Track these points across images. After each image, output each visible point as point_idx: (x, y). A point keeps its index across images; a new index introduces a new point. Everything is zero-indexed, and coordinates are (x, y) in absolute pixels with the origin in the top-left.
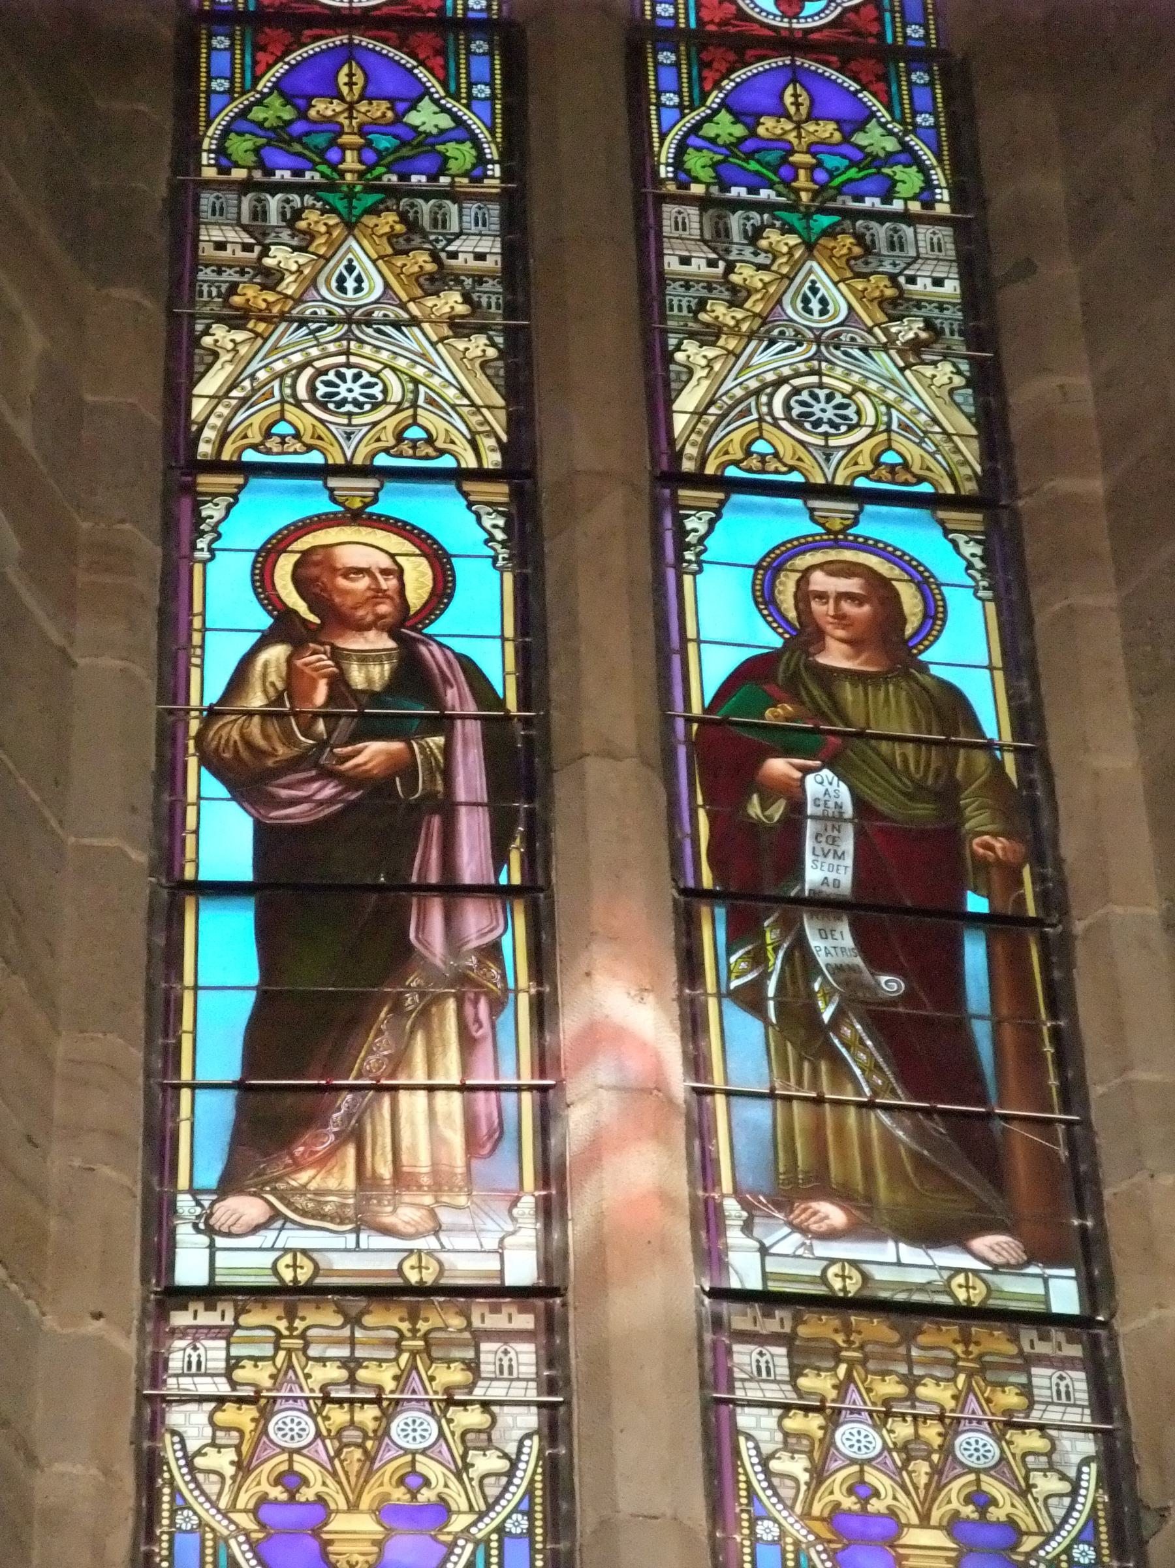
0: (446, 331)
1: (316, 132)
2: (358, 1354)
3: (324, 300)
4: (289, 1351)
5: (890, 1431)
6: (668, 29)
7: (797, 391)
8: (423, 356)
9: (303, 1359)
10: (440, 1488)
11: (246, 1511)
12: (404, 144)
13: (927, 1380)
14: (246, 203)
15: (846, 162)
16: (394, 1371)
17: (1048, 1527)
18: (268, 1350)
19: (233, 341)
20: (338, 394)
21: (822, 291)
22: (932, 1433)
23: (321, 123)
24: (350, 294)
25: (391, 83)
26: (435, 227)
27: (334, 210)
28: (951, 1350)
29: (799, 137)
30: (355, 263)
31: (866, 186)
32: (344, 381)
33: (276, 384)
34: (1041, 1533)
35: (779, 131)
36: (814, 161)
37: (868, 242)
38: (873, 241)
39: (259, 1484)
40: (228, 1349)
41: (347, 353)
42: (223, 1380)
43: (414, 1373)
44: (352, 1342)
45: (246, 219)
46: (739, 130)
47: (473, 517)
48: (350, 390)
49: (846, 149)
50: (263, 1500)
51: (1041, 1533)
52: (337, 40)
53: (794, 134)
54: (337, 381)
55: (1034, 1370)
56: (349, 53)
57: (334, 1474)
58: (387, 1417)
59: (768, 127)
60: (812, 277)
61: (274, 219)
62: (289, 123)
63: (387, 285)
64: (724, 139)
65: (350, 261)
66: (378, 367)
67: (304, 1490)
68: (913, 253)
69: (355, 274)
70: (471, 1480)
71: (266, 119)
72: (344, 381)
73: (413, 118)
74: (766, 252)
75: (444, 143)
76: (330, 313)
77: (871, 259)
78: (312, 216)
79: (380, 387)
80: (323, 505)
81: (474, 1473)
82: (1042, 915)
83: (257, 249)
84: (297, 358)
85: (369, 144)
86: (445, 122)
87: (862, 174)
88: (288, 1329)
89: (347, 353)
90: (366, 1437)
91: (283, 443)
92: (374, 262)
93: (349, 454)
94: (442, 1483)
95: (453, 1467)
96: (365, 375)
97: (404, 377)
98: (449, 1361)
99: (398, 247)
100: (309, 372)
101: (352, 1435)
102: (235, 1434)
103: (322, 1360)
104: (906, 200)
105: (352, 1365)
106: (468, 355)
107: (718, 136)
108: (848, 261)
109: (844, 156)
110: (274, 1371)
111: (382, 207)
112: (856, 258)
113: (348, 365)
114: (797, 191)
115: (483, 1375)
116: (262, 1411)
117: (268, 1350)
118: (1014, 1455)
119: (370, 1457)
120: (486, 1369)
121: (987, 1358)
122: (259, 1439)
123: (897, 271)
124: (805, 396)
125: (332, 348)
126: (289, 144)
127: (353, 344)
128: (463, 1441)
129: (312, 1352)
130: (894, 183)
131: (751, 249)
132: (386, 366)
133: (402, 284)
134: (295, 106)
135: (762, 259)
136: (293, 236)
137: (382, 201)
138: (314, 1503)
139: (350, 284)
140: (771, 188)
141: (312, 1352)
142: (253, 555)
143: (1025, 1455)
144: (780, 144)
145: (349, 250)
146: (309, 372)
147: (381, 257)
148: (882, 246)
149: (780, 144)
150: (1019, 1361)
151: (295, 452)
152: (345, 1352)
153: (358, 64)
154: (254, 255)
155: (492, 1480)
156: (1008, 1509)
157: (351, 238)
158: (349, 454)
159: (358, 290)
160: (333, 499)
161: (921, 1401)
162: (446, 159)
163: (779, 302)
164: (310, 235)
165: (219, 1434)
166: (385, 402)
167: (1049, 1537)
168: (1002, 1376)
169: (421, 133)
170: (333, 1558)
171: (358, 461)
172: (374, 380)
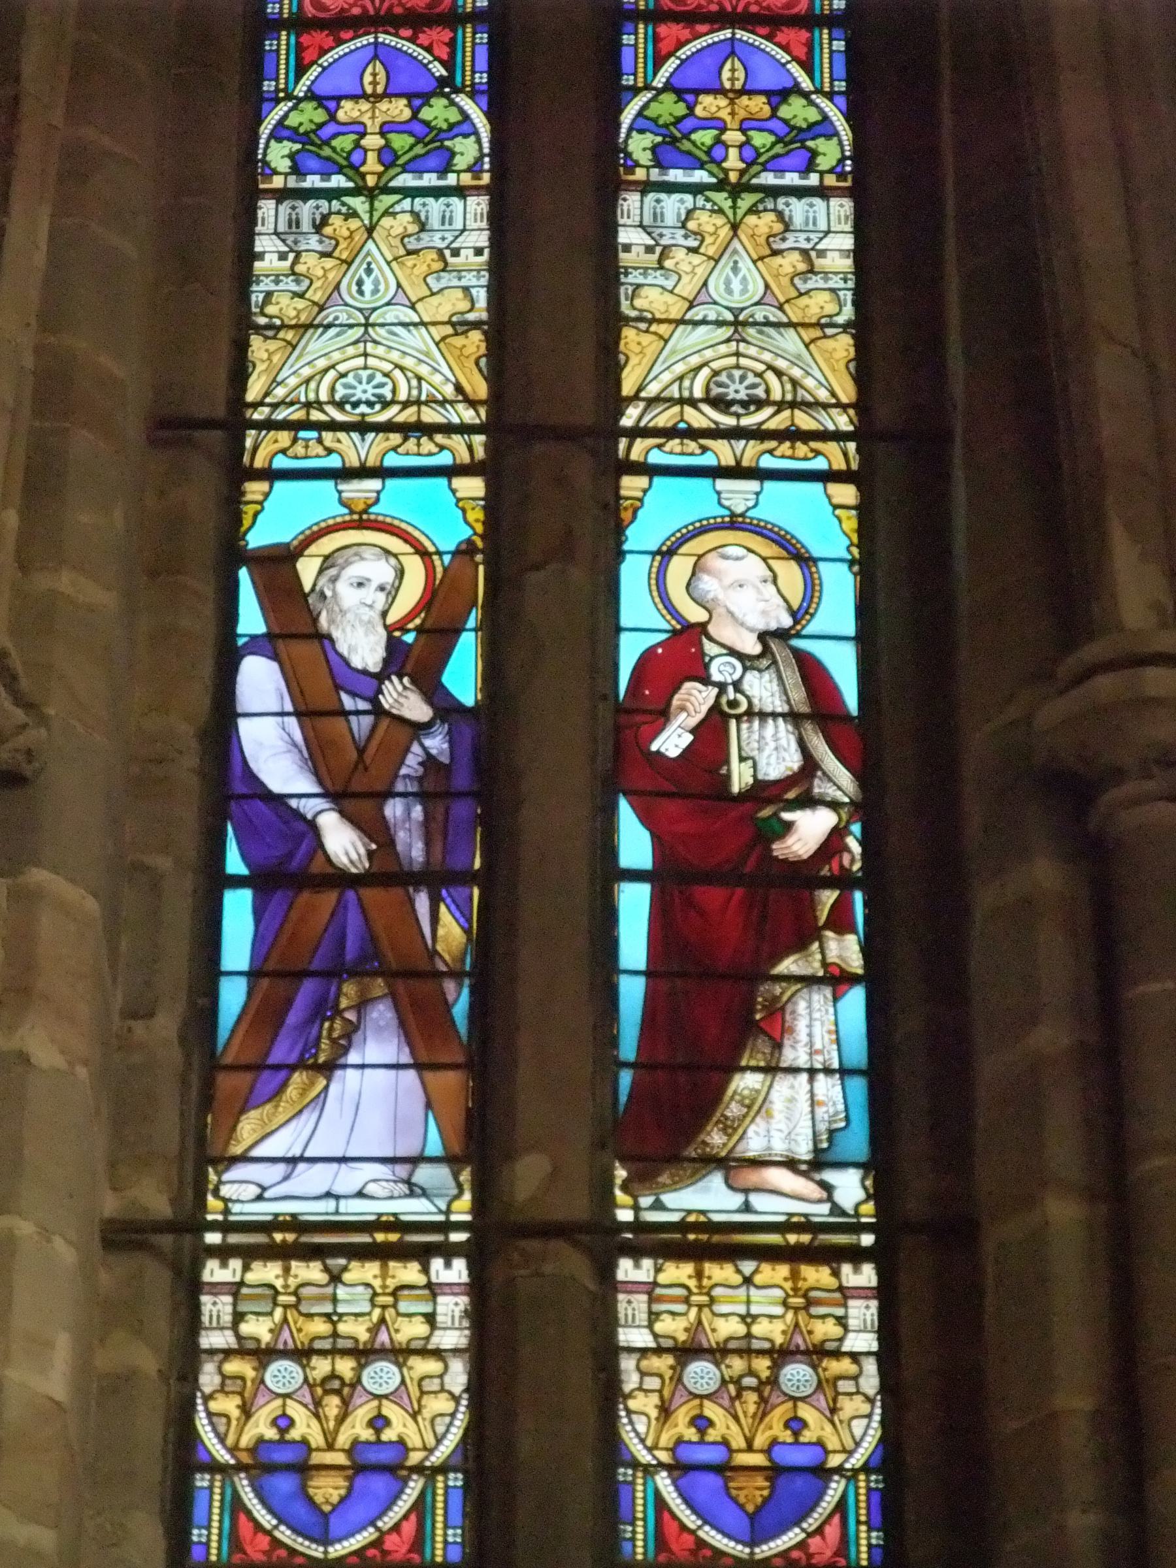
0: (449, 330)
1: (344, 134)
2: (340, 1310)
3: (346, 305)
4: (384, 1307)
5: (728, 1367)
6: (631, 10)
7: (716, 373)
8: (427, 354)
9: (807, 1318)
10: (724, 1431)
11: (667, 1449)
12: (780, 140)
13: (664, 1316)
14: (285, 208)
15: (772, 138)
16: (270, 1325)
17: (850, 1445)
18: (366, 1308)
19: (267, 350)
20: (353, 395)
21: (376, 272)
22: (762, 1365)
23: (351, 124)
24: (736, 296)
25: (768, 79)
26: (443, 223)
27: (721, 211)
28: (781, 1287)
29: (373, 117)
30: (373, 266)
31: (785, 162)
32: (733, 382)
33: (303, 388)
34: (425, 1448)
35: (714, 109)
36: (743, 138)
37: (423, 218)
38: (427, 218)
39: (353, 1427)
40: (235, 1305)
41: (366, 355)
42: (646, 1331)
43: (285, 1327)
44: (334, 1300)
45: (282, 228)
46: (681, 109)
47: (460, 512)
48: (365, 392)
49: (774, 124)
50: (680, 1442)
51: (844, 1451)
52: (364, 40)
53: (369, 114)
54: (355, 383)
55: (851, 1303)
56: (731, 49)
57: (736, 1418)
58: (776, 1367)
59: (348, 111)
60: (369, 259)
61: (306, 226)
62: (321, 126)
63: (767, 286)
64: (666, 119)
65: (369, 264)
66: (762, 367)
67: (710, 1431)
68: (824, 227)
69: (740, 275)
70: (841, 1422)
71: (301, 124)
72: (733, 382)
73: (426, 114)
74: (331, 238)
75: (452, 138)
76: (719, 314)
77: (423, 235)
78: (336, 220)
79: (390, 386)
80: (711, 510)
81: (427, 1414)
82: (20, 879)
83: (291, 256)
84: (322, 363)
85: (748, 142)
86: (454, 116)
87: (787, 149)
88: (792, 1289)
89: (737, 354)
90: (343, 1383)
91: (307, 447)
92: (388, 263)
93: (363, 458)
94: (724, 1426)
95: (410, 1410)
96: (750, 375)
97: (410, 374)
98: (823, 1317)
99: (409, 247)
100: (332, 374)
101: (749, 1381)
102: (239, 1382)
103: (310, 1316)
104: (822, 173)
105: (749, 1320)
106: (466, 352)
107: (660, 116)
108: (402, 240)
109: (771, 132)
110: (273, 1326)
111: (761, 207)
112: (774, 236)
113: (738, 367)
114: (726, 171)
115: (851, 1328)
116: (774, 1361)
117: (366, 1308)
118: (411, 1378)
119: (346, 1403)
120: (852, 1323)
121: (813, 1294)
122: (258, 1389)
123: (809, 246)
124: (350, 379)
125: (351, 351)
126: (320, 147)
127: (369, 345)
128: (420, 1386)
129: (304, 1308)
130: (814, 154)
131: (682, 232)
132: (397, 366)
133: (779, 286)
134: (327, 109)
135: (693, 243)
136: (686, 237)
137: (761, 201)
138: (397, 1442)
139: (368, 287)
140: (702, 167)
141: (304, 1308)
142: (321, 559)
143: (422, 1379)
144: (714, 123)
145: (368, 254)
146: (705, 373)
147: (395, 259)
148: (435, 222)
149: (714, 123)
150: (837, 1295)
151: (318, 456)
152: (742, 1310)
153: (739, 59)
154: (288, 263)
155: (438, 1420)
156: (819, 1433)
157: (370, 241)
158: (363, 458)
159: (375, 291)
160: (342, 502)
161: (757, 1338)
162: (452, 154)
163: (337, 287)
164: (699, 235)
165: (228, 1382)
166: (393, 402)
167: (850, 1453)
168: (822, 1310)
169: (434, 128)
170: (734, 1492)
171: (371, 463)
172: (758, 380)
